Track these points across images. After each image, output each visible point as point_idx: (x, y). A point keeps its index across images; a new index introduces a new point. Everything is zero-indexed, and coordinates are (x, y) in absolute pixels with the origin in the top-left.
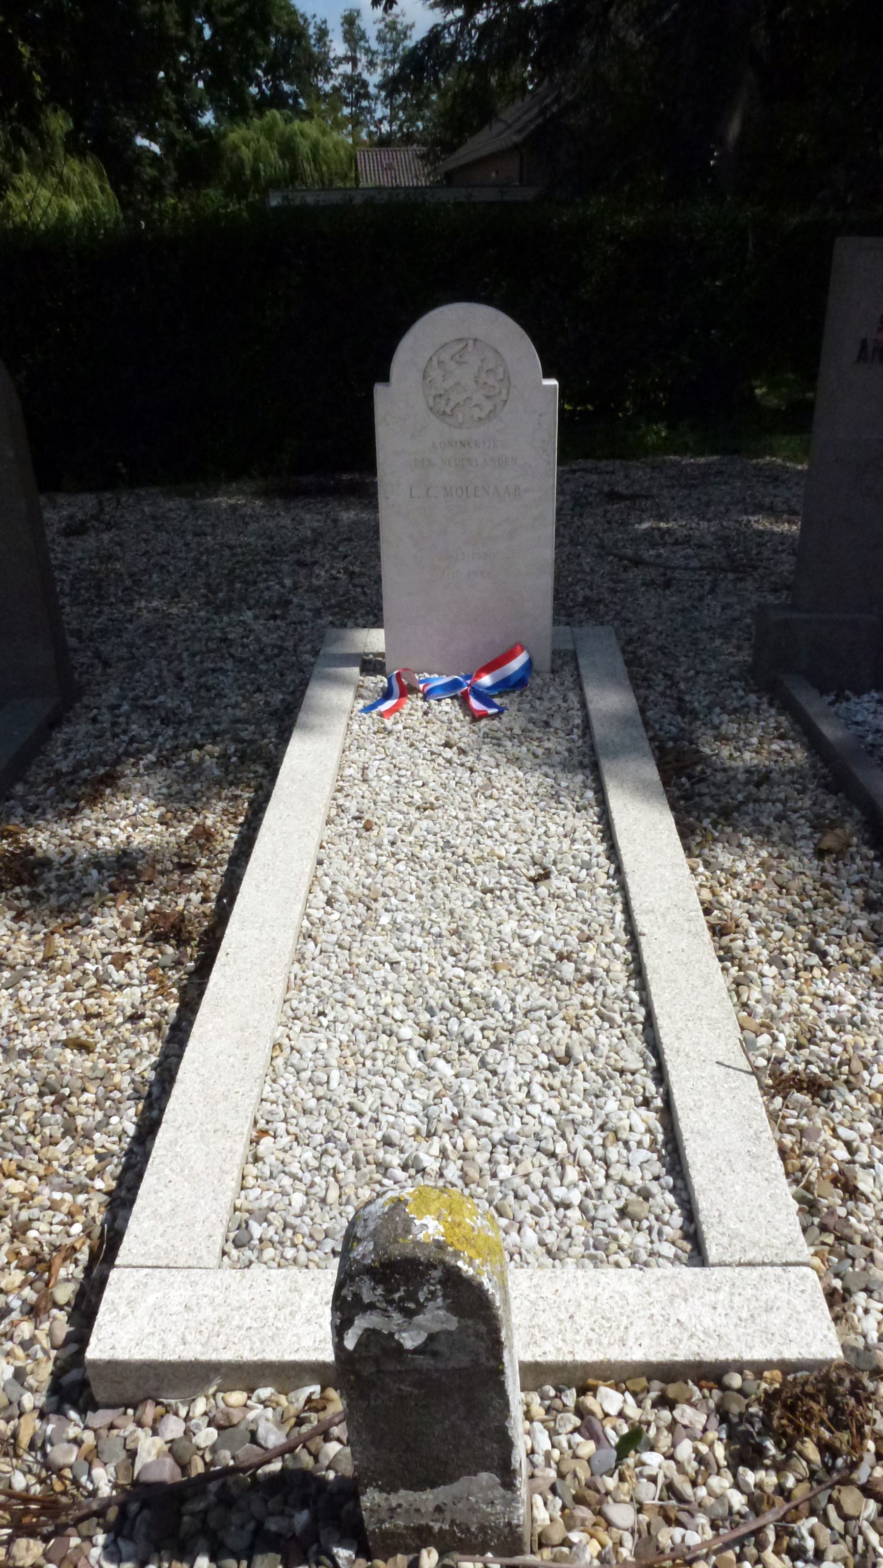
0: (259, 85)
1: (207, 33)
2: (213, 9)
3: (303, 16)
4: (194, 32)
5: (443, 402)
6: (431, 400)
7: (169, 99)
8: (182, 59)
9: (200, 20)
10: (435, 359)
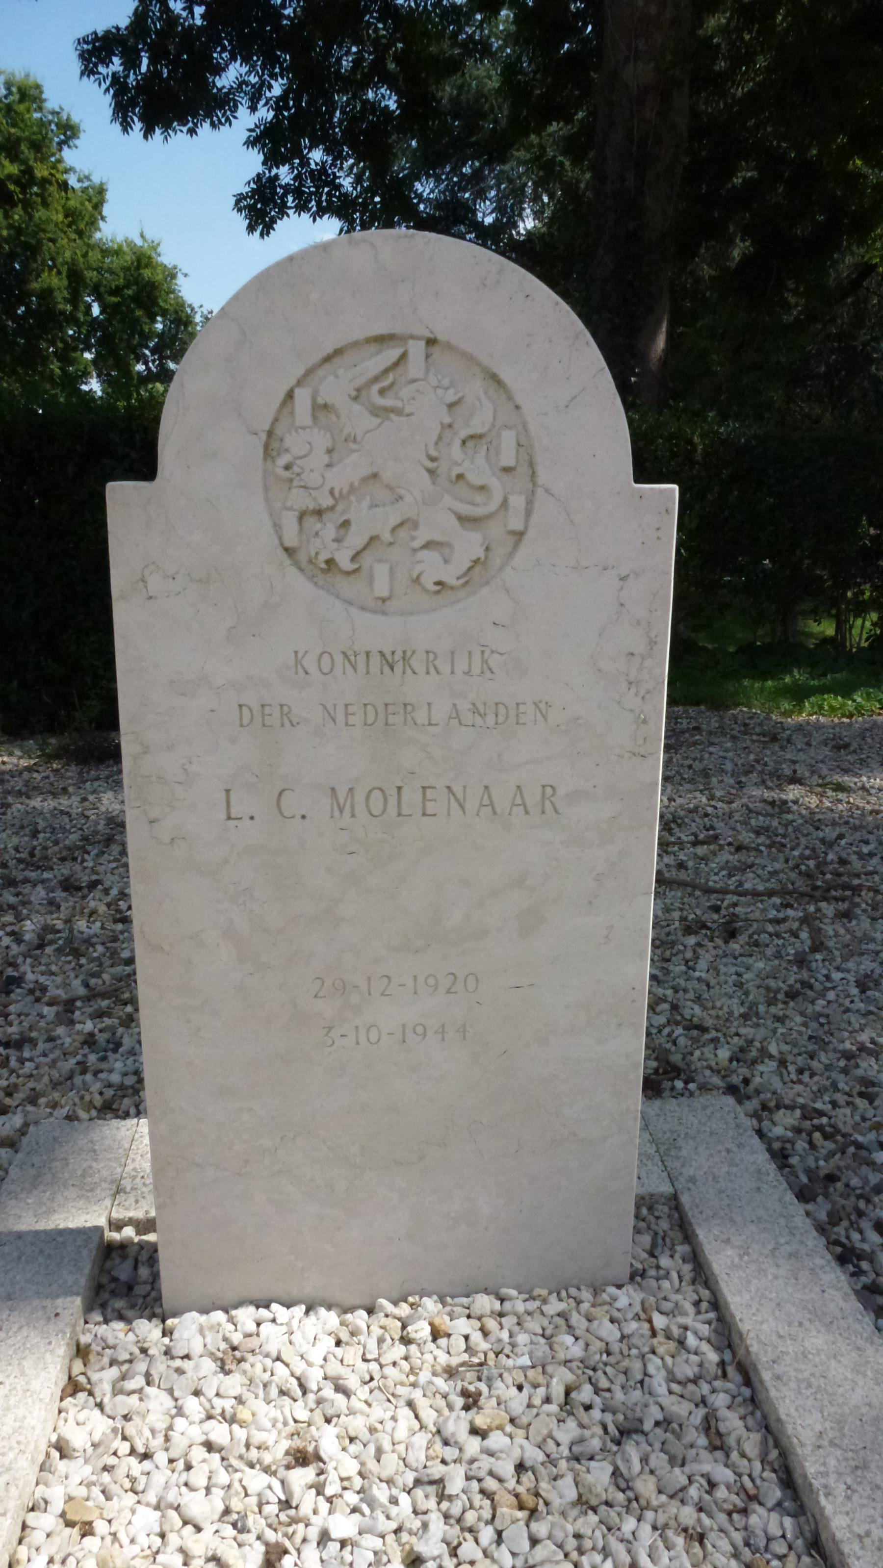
0: (146, 363)
1: (96, 310)
2: (102, 289)
3: (190, 306)
4: (82, 308)
5: (330, 531)
6: (290, 521)
7: (55, 367)
8: (71, 332)
9: (88, 299)
10: (303, 397)
